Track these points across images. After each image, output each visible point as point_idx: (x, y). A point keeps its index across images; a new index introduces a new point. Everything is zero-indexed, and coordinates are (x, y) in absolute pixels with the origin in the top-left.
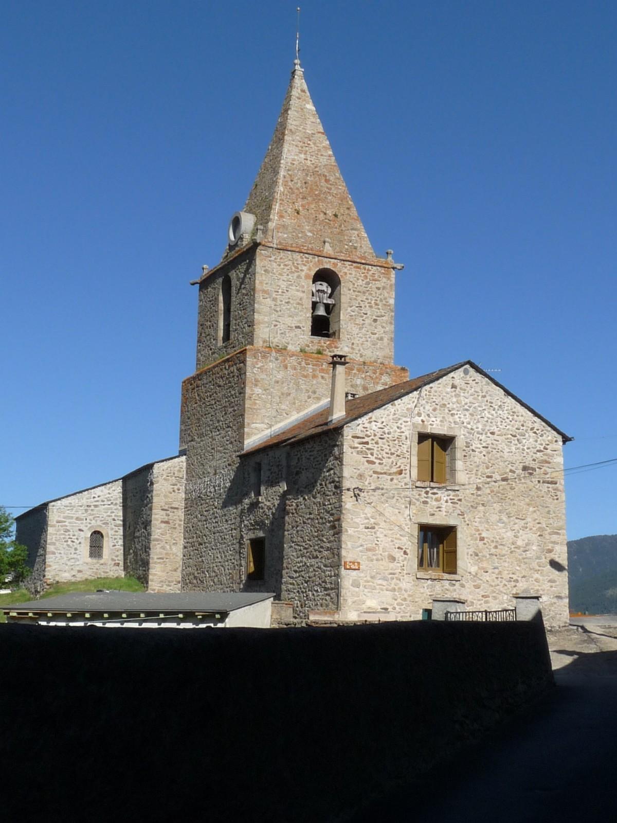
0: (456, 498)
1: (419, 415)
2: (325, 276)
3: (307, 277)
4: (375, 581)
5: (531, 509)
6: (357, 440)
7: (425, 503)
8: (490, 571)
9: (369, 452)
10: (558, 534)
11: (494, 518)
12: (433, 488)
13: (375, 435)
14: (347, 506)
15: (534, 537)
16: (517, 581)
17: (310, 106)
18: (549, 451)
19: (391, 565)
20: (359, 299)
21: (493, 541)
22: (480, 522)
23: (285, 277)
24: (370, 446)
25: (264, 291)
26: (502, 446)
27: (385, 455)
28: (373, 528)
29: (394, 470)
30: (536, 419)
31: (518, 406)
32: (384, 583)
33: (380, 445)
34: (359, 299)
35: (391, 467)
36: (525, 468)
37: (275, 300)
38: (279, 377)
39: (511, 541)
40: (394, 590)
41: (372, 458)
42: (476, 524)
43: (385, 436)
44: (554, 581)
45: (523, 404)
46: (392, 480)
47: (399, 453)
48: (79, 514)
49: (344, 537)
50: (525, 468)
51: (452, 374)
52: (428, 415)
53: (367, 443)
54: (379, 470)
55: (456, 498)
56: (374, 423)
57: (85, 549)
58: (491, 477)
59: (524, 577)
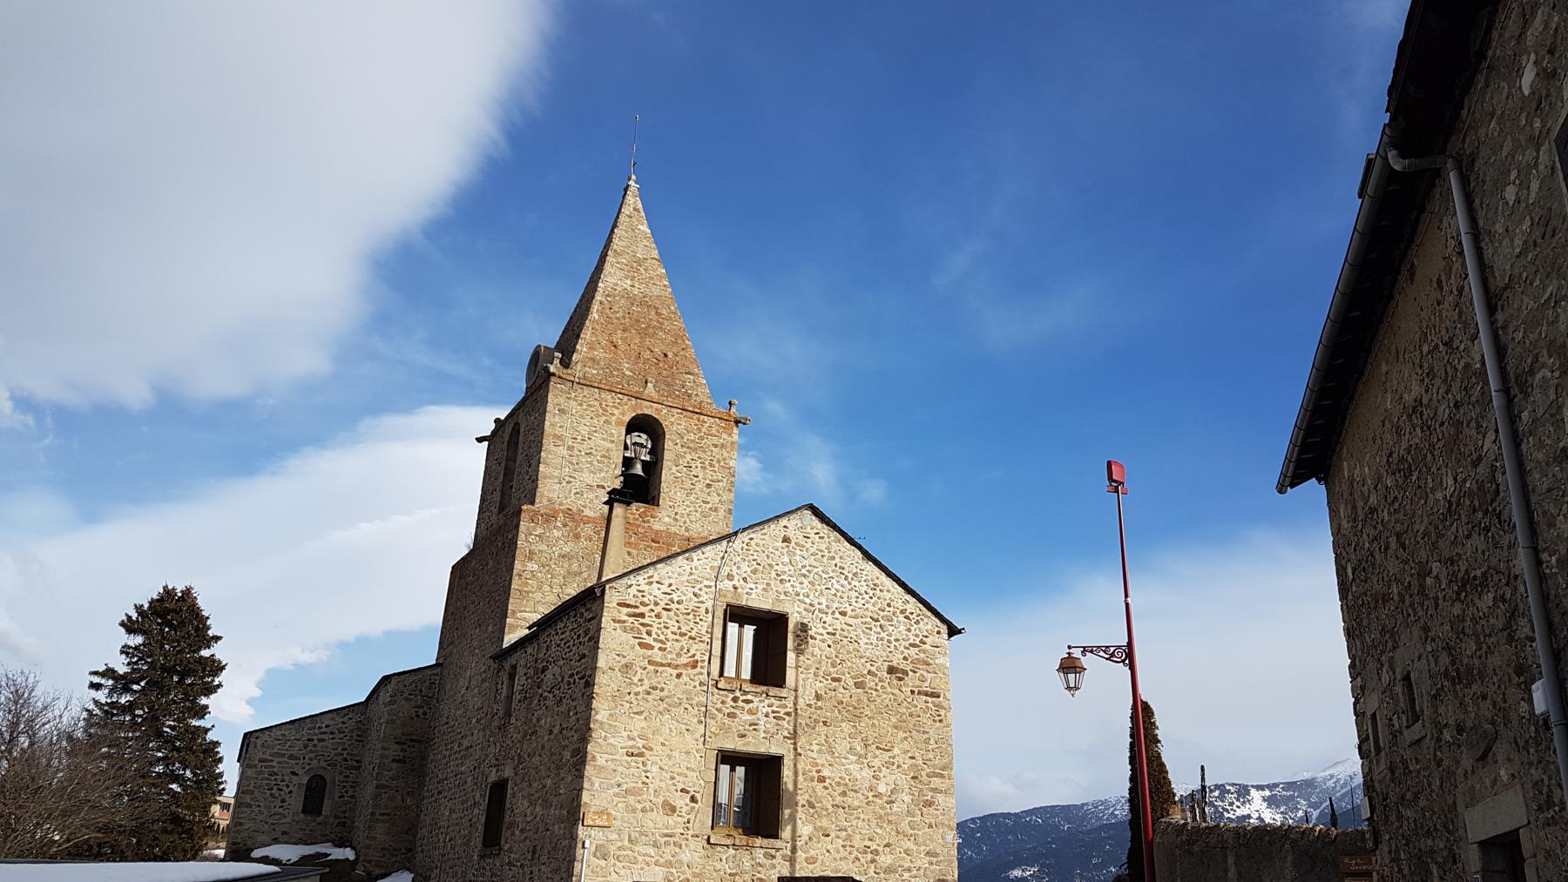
0: (783, 711)
1: (730, 577)
2: (642, 424)
3: (618, 423)
4: (637, 848)
5: (901, 734)
6: (625, 610)
7: (731, 715)
8: (833, 835)
9: (644, 630)
10: (942, 776)
11: (841, 747)
12: (746, 693)
13: (656, 604)
14: (599, 717)
15: (904, 781)
16: (876, 852)
17: (644, 228)
18: (927, 647)
19: (671, 820)
20: (689, 457)
21: (839, 784)
22: (820, 751)
23: (587, 421)
24: (646, 620)
25: (556, 437)
26: (857, 632)
27: (671, 637)
28: (641, 755)
29: (684, 660)
30: (908, 597)
31: (883, 577)
32: (652, 851)
33: (664, 619)
34: (689, 457)
35: (678, 655)
36: (891, 670)
37: (570, 448)
38: (567, 549)
39: (867, 785)
40: (669, 864)
41: (649, 640)
42: (814, 755)
43: (674, 606)
44: (936, 855)
45: (890, 574)
46: (679, 676)
47: (693, 634)
48: (294, 752)
49: (589, 770)
50: (891, 670)
51: (784, 522)
52: (745, 579)
53: (642, 615)
54: (658, 660)
55: (783, 711)
56: (656, 586)
57: (296, 801)
58: (838, 680)
59: (888, 845)
